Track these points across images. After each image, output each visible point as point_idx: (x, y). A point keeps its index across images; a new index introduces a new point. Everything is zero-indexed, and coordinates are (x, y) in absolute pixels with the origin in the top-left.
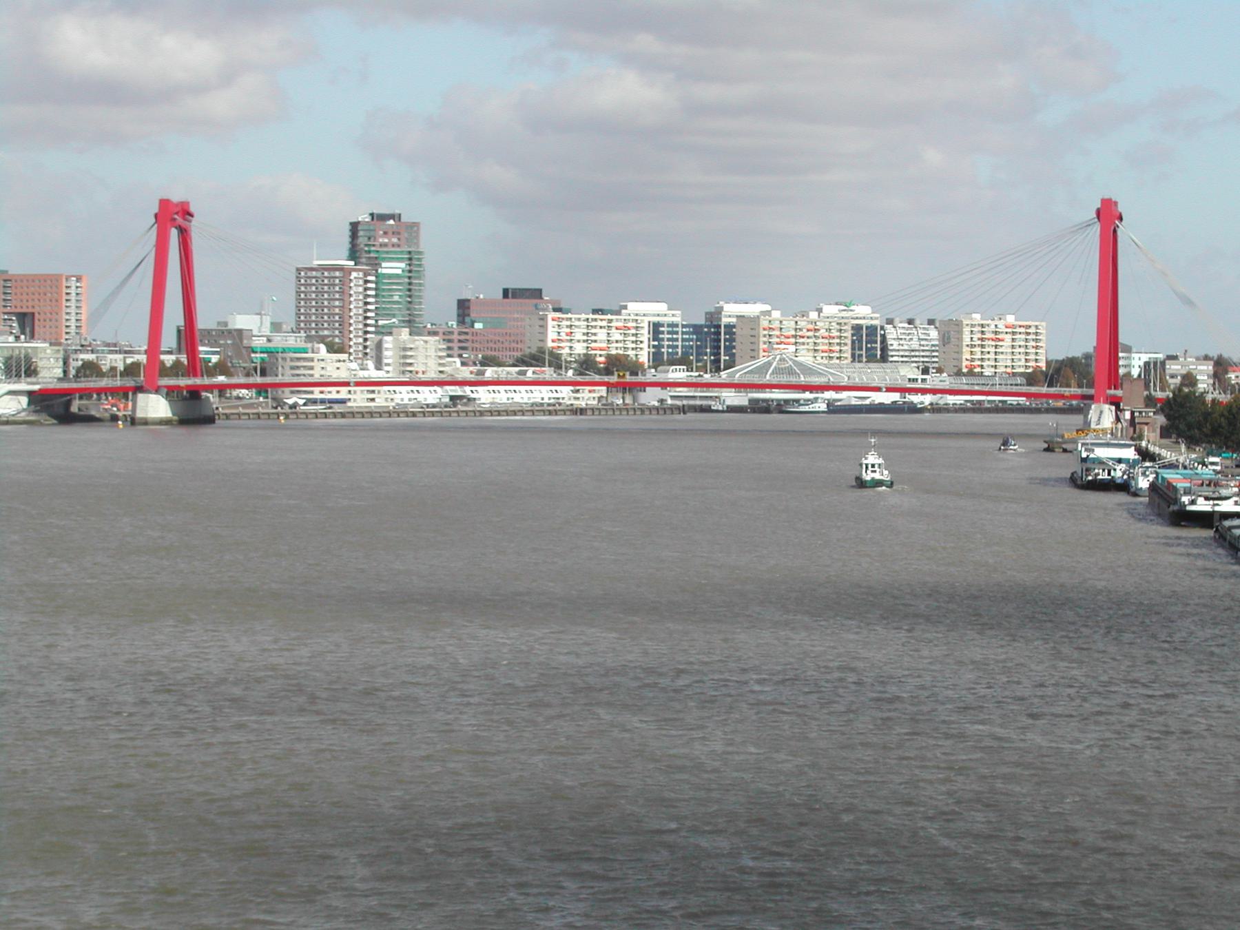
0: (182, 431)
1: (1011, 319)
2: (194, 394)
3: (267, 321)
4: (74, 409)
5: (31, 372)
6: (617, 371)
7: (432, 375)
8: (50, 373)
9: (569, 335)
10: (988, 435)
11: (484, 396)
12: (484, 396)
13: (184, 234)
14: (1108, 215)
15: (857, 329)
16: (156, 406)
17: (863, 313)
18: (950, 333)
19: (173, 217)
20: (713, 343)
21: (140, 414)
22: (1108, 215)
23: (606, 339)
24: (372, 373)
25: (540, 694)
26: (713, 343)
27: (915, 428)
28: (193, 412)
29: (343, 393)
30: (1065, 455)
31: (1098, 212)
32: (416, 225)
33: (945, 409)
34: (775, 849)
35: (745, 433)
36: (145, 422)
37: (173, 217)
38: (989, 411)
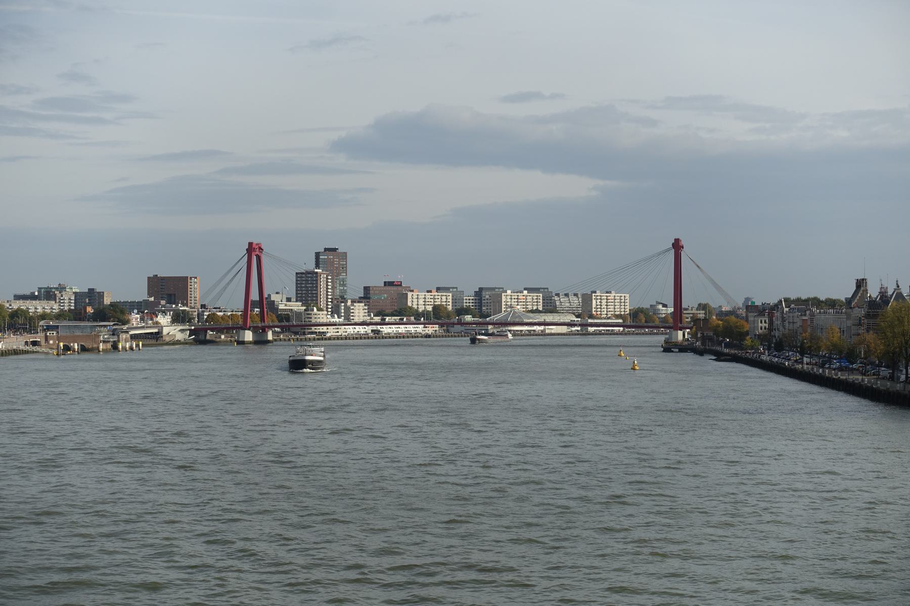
0: (256, 347)
4: (208, 337)
5: (190, 321)
10: (549, 345)
11: (386, 329)
12: (386, 329)
14: (677, 246)
18: (587, 299)
19: (253, 250)
22: (677, 246)
24: (336, 319)
27: (592, 343)
29: (324, 329)
30: (240, 347)
31: (673, 244)
32: (346, 253)
33: (613, 333)
35: (396, 345)
37: (253, 250)
38: (617, 334)
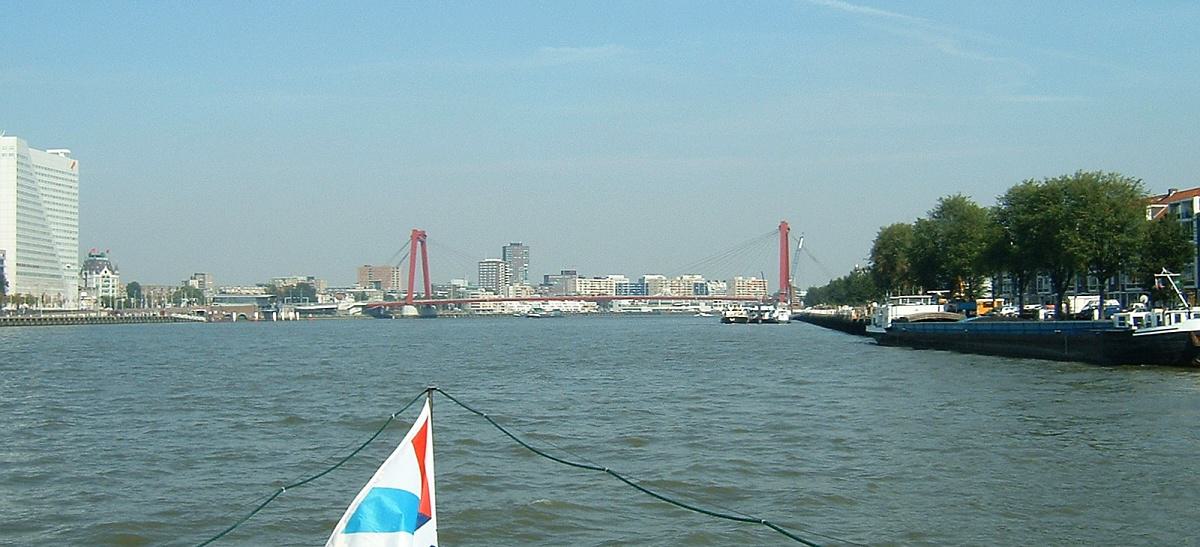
1: (754, 279)
2: (428, 305)
3: (466, 281)
6: (603, 301)
7: (514, 298)
8: (378, 298)
9: (581, 287)
13: (423, 243)
14: (784, 229)
15: (696, 285)
16: (411, 311)
17: (698, 279)
19: (419, 237)
20: (640, 290)
21: (405, 314)
22: (784, 229)
23: (601, 288)
25: (196, 417)
26: (640, 290)
28: (427, 312)
34: (245, 534)
36: (408, 316)
37: (419, 237)
